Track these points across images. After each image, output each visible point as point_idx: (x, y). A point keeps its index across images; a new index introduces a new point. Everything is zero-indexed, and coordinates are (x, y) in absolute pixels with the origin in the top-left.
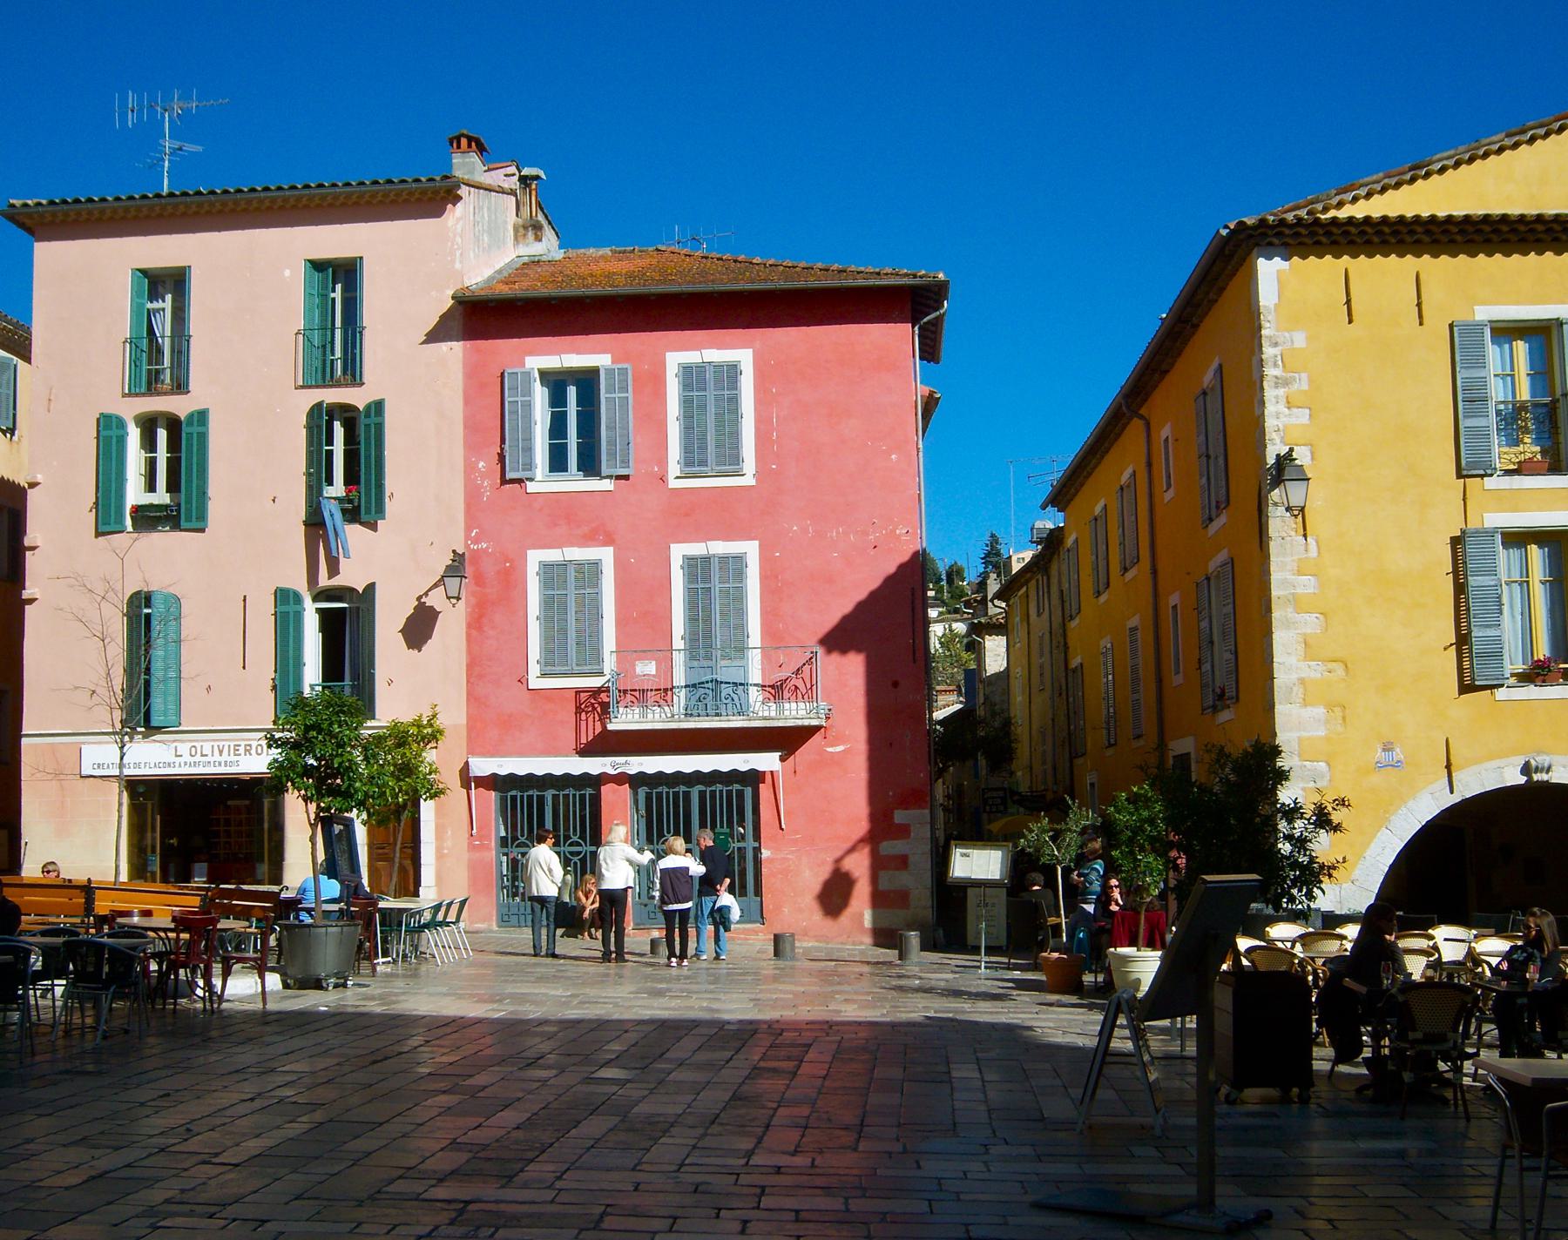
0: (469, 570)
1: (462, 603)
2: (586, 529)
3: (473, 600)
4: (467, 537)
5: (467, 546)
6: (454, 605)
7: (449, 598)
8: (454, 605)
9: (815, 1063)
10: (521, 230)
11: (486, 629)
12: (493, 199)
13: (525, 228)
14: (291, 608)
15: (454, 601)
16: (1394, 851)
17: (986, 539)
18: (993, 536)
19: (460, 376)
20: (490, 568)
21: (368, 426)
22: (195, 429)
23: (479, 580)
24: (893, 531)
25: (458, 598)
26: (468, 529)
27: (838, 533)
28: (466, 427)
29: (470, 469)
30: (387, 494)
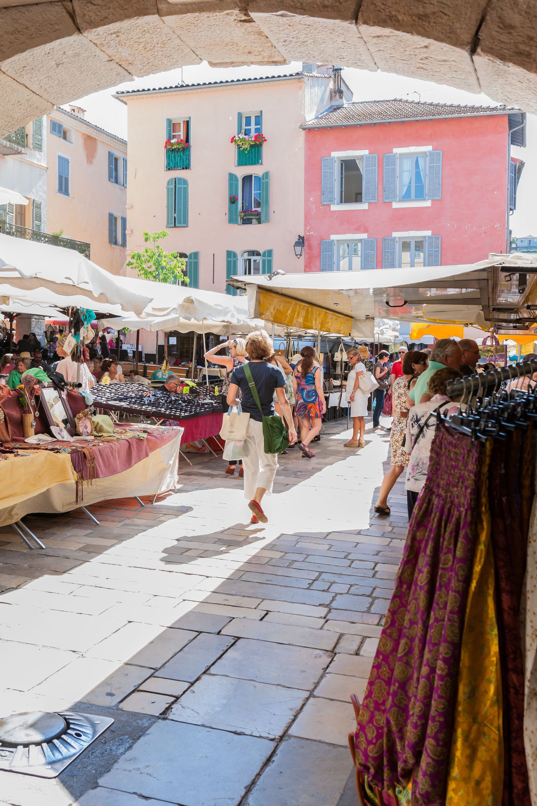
0: (306, 243)
1: (303, 257)
2: (355, 226)
3: (307, 256)
4: (305, 230)
5: (305, 233)
6: (299, 258)
7: (296, 255)
8: (299, 258)
9: (433, 455)
10: (334, 94)
11: (312, 268)
12: (320, 81)
13: (335, 92)
14: (232, 259)
15: (299, 256)
16: (143, 709)
17: (150, 297)
18: (152, 299)
19: (303, 161)
20: (315, 243)
21: (263, 183)
22: (265, 181)
23: (310, 247)
24: (494, 226)
25: (301, 255)
26: (306, 226)
27: (468, 226)
28: (305, 183)
29: (307, 200)
30: (227, 215)
